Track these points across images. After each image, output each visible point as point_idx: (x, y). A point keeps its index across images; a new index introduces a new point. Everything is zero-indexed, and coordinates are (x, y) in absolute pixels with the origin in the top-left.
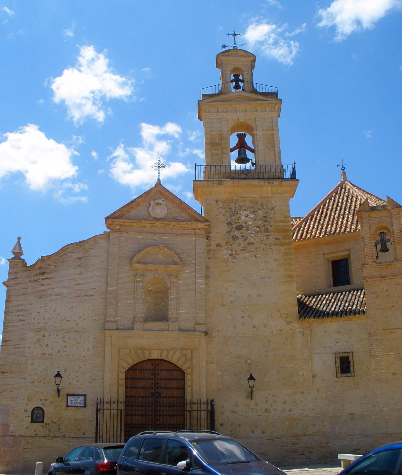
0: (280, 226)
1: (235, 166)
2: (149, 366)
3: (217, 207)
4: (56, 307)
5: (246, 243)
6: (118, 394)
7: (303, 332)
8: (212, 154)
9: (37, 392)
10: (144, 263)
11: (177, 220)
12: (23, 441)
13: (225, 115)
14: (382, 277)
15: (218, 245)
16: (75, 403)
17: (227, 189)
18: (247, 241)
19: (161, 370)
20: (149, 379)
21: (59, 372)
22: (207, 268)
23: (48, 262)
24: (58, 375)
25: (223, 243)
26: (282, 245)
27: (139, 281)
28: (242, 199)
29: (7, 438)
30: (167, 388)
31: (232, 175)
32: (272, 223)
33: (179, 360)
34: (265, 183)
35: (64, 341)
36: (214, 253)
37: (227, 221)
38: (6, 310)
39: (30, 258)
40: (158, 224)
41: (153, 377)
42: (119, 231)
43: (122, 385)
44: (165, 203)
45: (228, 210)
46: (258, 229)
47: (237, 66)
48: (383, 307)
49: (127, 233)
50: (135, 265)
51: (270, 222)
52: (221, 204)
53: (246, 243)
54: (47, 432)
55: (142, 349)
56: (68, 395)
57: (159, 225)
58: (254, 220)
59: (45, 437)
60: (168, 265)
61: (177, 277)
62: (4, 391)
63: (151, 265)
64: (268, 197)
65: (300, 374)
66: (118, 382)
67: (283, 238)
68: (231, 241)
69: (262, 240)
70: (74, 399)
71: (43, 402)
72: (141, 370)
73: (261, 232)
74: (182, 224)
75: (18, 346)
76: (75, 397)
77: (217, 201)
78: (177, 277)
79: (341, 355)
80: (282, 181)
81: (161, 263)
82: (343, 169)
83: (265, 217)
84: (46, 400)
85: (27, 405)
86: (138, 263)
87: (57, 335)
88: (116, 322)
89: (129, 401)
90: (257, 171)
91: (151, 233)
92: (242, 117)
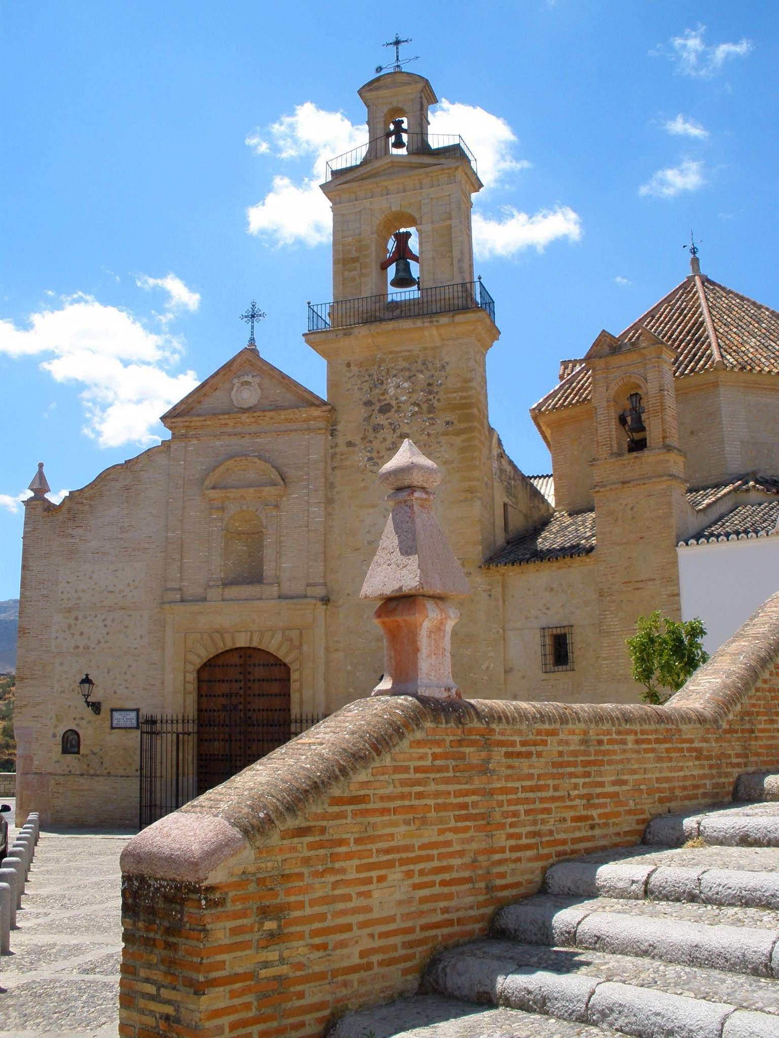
0: (455, 398)
1: (396, 294)
2: (236, 660)
3: (351, 375)
4: (93, 572)
5: (395, 436)
6: (185, 707)
7: (490, 590)
8: (344, 280)
9: (69, 706)
10: (221, 488)
11: (278, 408)
12: (52, 782)
13: (366, 203)
14: (623, 483)
15: (350, 444)
16: (122, 723)
17: (362, 342)
18: (398, 432)
19: (255, 665)
20: (236, 681)
21: (87, 675)
22: (331, 486)
23: (80, 500)
24: (87, 681)
25: (357, 439)
26: (458, 433)
27: (215, 519)
28: (390, 356)
29: (30, 777)
30: (263, 695)
31: (377, 314)
32: (441, 395)
33: (279, 648)
34: (423, 323)
35: (105, 626)
36: (341, 459)
37: (364, 399)
38: (22, 582)
39: (56, 497)
40: (244, 417)
41: (241, 677)
42: (185, 436)
43: (190, 693)
44: (257, 380)
45: (367, 378)
46: (416, 409)
47: (395, 104)
48: (624, 540)
49: (198, 439)
50: (207, 492)
51: (437, 393)
52: (354, 369)
53: (395, 436)
54: (85, 767)
55: (221, 632)
56: (112, 710)
57: (248, 421)
58: (409, 393)
59: (82, 775)
60: (261, 488)
61: (277, 507)
62: (25, 706)
63: (233, 490)
64: (434, 348)
65: (484, 667)
66: (185, 688)
67: (459, 421)
68: (371, 435)
69: (423, 426)
70: (121, 717)
71: (77, 721)
72: (223, 666)
73: (421, 413)
74: (283, 415)
75: (40, 637)
76: (123, 713)
77: (349, 365)
78: (277, 507)
79: (555, 632)
80: (453, 316)
81: (250, 486)
82: (694, 251)
83: (429, 385)
84: (82, 719)
85: (56, 726)
86: (214, 488)
87: (96, 616)
88: (180, 589)
89: (204, 719)
90: (425, 300)
91: (235, 435)
92: (395, 203)
